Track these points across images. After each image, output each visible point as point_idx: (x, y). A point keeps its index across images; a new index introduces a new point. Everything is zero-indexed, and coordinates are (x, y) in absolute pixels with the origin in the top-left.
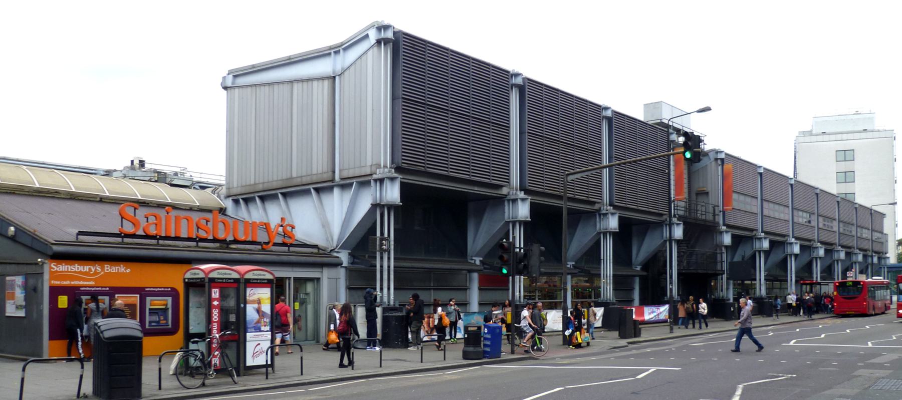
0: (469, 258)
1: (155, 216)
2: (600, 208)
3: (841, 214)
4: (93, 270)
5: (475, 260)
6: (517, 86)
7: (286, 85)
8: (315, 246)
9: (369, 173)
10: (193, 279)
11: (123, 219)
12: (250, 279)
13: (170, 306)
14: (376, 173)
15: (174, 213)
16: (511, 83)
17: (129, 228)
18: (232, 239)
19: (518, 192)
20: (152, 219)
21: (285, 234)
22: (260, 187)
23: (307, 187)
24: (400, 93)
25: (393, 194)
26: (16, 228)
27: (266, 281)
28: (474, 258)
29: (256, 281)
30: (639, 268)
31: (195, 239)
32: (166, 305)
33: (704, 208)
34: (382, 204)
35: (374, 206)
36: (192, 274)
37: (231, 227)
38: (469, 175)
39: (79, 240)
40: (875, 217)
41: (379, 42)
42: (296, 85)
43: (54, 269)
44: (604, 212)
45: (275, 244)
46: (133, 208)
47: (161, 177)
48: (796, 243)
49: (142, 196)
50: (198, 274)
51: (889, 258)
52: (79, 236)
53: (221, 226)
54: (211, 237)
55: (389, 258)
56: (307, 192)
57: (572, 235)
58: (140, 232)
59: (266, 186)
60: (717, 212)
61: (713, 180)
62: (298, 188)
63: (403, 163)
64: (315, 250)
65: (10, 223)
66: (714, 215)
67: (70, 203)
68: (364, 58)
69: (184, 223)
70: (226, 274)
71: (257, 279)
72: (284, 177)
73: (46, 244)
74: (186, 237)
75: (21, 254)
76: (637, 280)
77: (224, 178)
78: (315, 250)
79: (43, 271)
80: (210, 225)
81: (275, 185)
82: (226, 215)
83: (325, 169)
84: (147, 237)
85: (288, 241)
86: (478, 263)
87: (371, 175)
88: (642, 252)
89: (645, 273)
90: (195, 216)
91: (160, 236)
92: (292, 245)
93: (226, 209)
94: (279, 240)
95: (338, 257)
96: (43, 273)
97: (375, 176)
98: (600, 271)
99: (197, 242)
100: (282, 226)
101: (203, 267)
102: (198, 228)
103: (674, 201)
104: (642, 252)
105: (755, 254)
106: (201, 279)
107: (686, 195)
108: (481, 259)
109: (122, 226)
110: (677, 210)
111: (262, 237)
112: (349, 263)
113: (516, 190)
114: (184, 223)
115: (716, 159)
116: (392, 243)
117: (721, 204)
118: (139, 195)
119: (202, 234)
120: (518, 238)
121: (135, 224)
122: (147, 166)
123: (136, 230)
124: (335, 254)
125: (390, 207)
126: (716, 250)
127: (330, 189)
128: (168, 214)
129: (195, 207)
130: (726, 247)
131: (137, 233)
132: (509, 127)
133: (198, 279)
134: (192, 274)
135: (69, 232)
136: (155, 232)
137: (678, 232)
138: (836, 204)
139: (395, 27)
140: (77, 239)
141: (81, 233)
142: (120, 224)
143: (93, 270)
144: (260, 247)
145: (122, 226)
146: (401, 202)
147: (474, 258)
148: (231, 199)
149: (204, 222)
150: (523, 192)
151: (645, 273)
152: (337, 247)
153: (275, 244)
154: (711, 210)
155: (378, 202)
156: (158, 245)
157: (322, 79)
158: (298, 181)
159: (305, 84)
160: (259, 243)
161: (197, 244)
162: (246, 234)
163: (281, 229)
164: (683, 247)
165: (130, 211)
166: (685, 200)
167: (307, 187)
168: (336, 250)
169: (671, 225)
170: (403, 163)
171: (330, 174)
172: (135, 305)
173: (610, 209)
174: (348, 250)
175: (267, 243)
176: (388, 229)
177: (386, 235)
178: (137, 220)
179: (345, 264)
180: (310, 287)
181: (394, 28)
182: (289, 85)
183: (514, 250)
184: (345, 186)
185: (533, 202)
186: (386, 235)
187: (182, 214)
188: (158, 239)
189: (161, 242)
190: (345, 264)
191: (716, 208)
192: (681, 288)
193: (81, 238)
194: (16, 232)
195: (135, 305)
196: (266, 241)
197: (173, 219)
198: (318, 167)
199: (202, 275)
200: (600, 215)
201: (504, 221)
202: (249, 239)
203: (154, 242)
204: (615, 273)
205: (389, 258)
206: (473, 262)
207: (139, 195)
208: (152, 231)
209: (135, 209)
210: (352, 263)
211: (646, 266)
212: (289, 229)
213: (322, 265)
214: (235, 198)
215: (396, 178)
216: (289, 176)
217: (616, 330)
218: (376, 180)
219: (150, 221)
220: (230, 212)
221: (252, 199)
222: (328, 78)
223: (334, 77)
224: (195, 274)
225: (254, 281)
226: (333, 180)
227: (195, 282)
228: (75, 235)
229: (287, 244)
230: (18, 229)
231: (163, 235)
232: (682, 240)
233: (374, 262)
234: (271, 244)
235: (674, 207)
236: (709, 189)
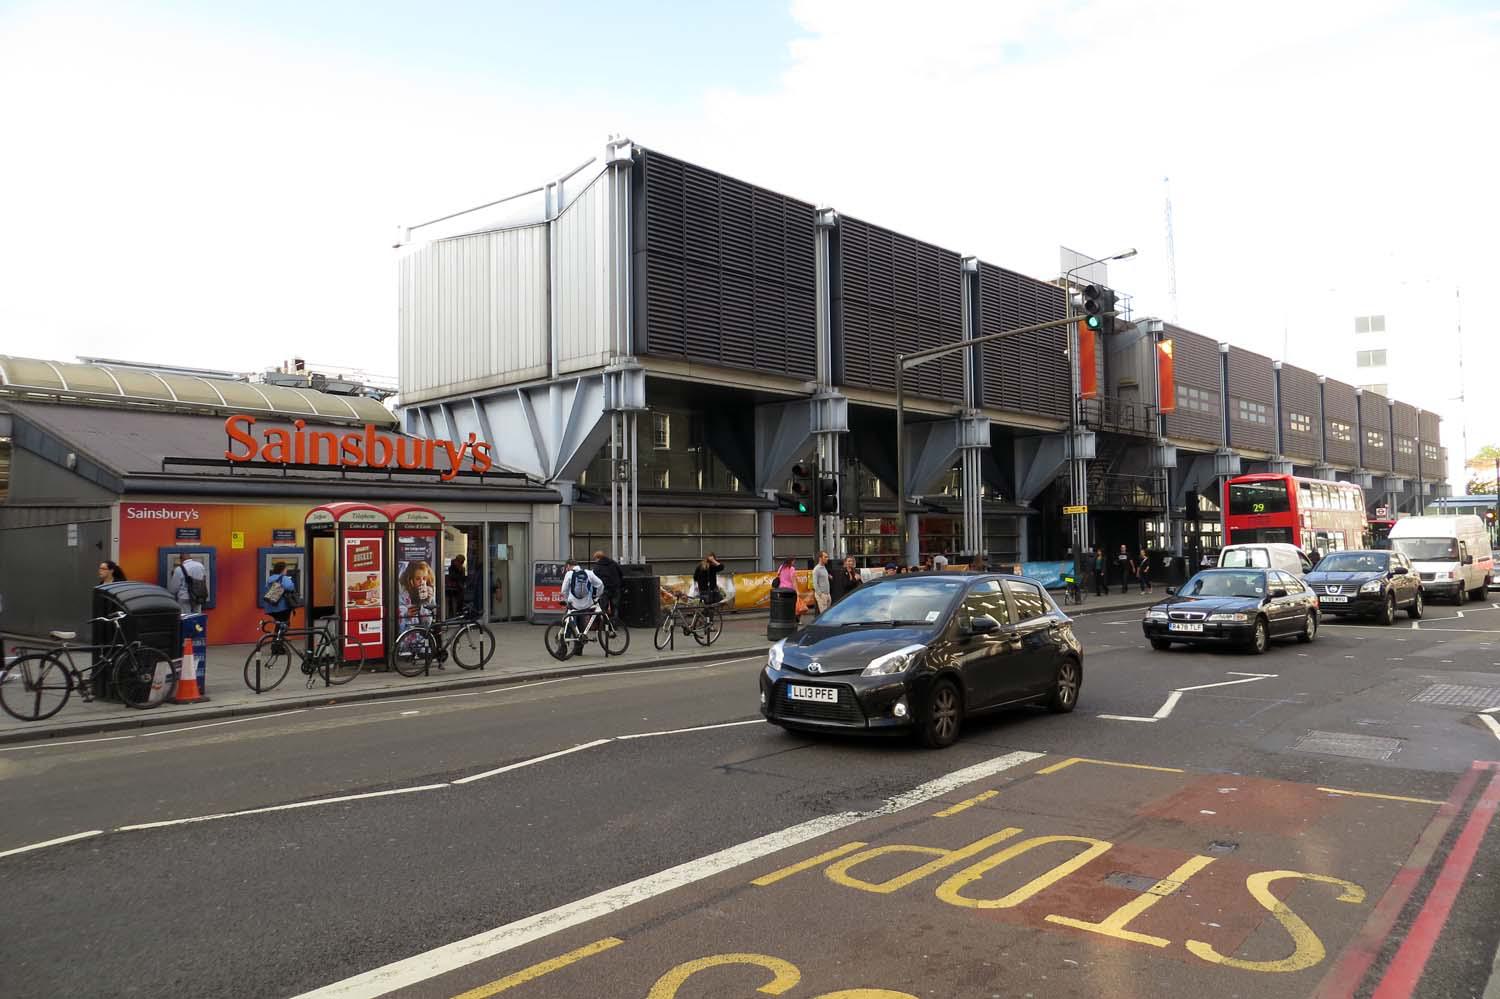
0: (757, 490)
1: (382, 442)
2: (961, 412)
3: (1363, 417)
4: (188, 517)
5: (766, 494)
6: (826, 227)
7: (480, 237)
8: (522, 476)
9: (599, 363)
10: (317, 524)
11: (233, 440)
12: (349, 523)
13: (301, 566)
14: (609, 365)
15: (308, 430)
16: (816, 223)
17: (240, 451)
18: (396, 465)
19: (830, 389)
20: (275, 439)
21: (476, 457)
22: (446, 391)
23: (512, 388)
24: (642, 241)
25: (636, 395)
26: (77, 456)
27: (376, 527)
28: (765, 491)
29: (358, 526)
30: (1026, 504)
31: (228, 461)
32: (297, 565)
33: (1130, 410)
34: (619, 409)
35: (608, 413)
36: (316, 517)
37: (395, 448)
38: (718, 359)
39: (166, 471)
40: (1425, 424)
41: (611, 166)
42: (494, 237)
43: (131, 515)
44: (968, 418)
45: (460, 473)
46: (246, 424)
47: (319, 383)
48: (1086, 435)
49: (275, 408)
50: (324, 517)
51: (1449, 486)
52: (166, 466)
53: (379, 447)
54: (364, 464)
55: (630, 492)
56: (512, 395)
57: (917, 457)
58: (258, 458)
59: (455, 389)
60: (1151, 416)
61: (1142, 368)
62: (500, 390)
63: (651, 348)
64: (522, 482)
65: (70, 448)
66: (1148, 421)
67: (167, 419)
68: (589, 192)
69: (324, 443)
70: (366, 516)
71: (361, 524)
72: (480, 375)
73: (117, 477)
74: (327, 464)
75: (87, 494)
76: (1024, 521)
77: (396, 381)
78: (522, 482)
79: (110, 516)
80: (362, 446)
81: (467, 387)
82: (400, 433)
83: (537, 362)
84: (371, 469)
85: (481, 466)
86: (771, 497)
87: (603, 367)
88: (1030, 479)
89: (1035, 512)
90: (340, 435)
91: (288, 464)
92: (487, 474)
93: (399, 423)
94: (466, 466)
95: (555, 491)
96: (110, 520)
97: (608, 369)
98: (963, 508)
99: (343, 471)
100: (470, 445)
101: (333, 506)
102: (344, 450)
103: (1080, 399)
104: (1030, 479)
105: (1218, 480)
106: (328, 524)
107: (1101, 391)
108: (776, 491)
109: (230, 450)
110: (1086, 413)
111: (441, 462)
112: (573, 500)
113: (827, 384)
114: (324, 443)
115: (1150, 334)
116: (635, 468)
117: (1159, 403)
118: (121, 391)
119: (351, 459)
120: (828, 454)
121: (251, 445)
122: (307, 368)
123: (252, 455)
124: (552, 487)
125: (631, 413)
126: (1152, 475)
127: (545, 389)
128: (299, 429)
129: (353, 422)
130: (1170, 470)
131: (253, 460)
132: (961, 327)
133: (324, 524)
134: (316, 517)
135: (152, 462)
136: (280, 457)
137: (1088, 447)
138: (1356, 399)
139: (635, 143)
140: (163, 468)
141: (168, 461)
142: (228, 447)
143: (188, 517)
144: (437, 478)
145: (230, 450)
146: (646, 406)
147: (765, 491)
148: (406, 409)
149: (353, 442)
150: (836, 389)
151: (1035, 512)
152: (554, 476)
153: (460, 473)
154: (1143, 413)
155: (613, 407)
156: (441, 482)
157: (532, 226)
158: (499, 380)
159: (507, 234)
160: (437, 472)
161: (344, 475)
162: (417, 456)
163: (469, 450)
164: (1097, 472)
165: (242, 427)
166: (1098, 398)
167: (512, 388)
168: (554, 481)
169: (1073, 437)
170: (651, 348)
171: (544, 367)
172: (348, 570)
173: (977, 413)
174: (572, 480)
175: (448, 472)
176: (625, 444)
177: (625, 457)
178: (254, 441)
179: (567, 500)
180: (514, 536)
181: (633, 145)
182: (486, 238)
183: (816, 475)
184: (565, 386)
185: (852, 404)
186: (625, 457)
187: (320, 430)
188: (285, 469)
189: (290, 472)
190: (567, 500)
191: (1151, 410)
192: (986, 526)
193: (170, 468)
194: (77, 460)
195: (348, 570)
196: (448, 468)
197: (307, 438)
198: (528, 362)
199: (329, 519)
200: (961, 422)
201: (808, 434)
202: (423, 465)
203: (279, 472)
204: (986, 511)
205: (630, 492)
206: (763, 496)
207: (121, 391)
208: (276, 455)
209: (249, 424)
210: (580, 500)
211: (1037, 502)
212: (482, 450)
213: (532, 502)
214: (412, 407)
215: (842, 399)
216: (487, 373)
217: (317, 608)
218: (609, 375)
219: (272, 441)
220: (404, 428)
221: (436, 409)
222: (540, 224)
223: (549, 224)
224: (320, 517)
225: (355, 527)
226: (549, 376)
227: (321, 530)
228: (160, 463)
229: (479, 473)
230: (82, 457)
231: (293, 461)
232: (1096, 461)
233: (609, 499)
234: (454, 473)
235: (1081, 408)
236: (1138, 380)
